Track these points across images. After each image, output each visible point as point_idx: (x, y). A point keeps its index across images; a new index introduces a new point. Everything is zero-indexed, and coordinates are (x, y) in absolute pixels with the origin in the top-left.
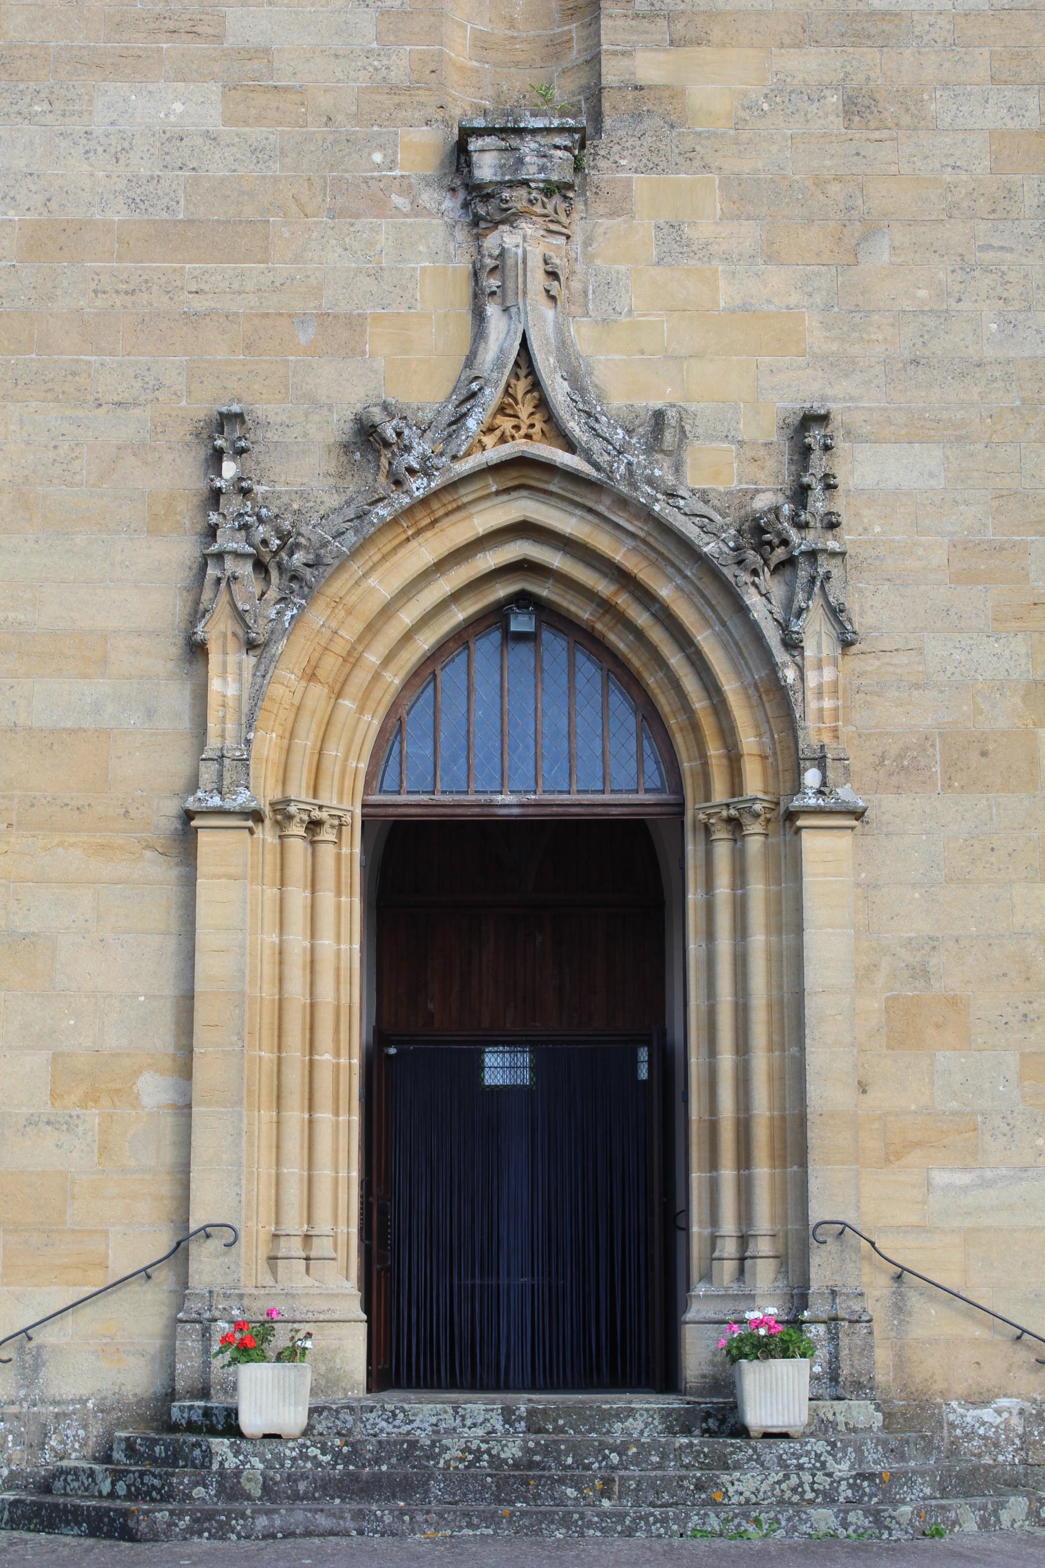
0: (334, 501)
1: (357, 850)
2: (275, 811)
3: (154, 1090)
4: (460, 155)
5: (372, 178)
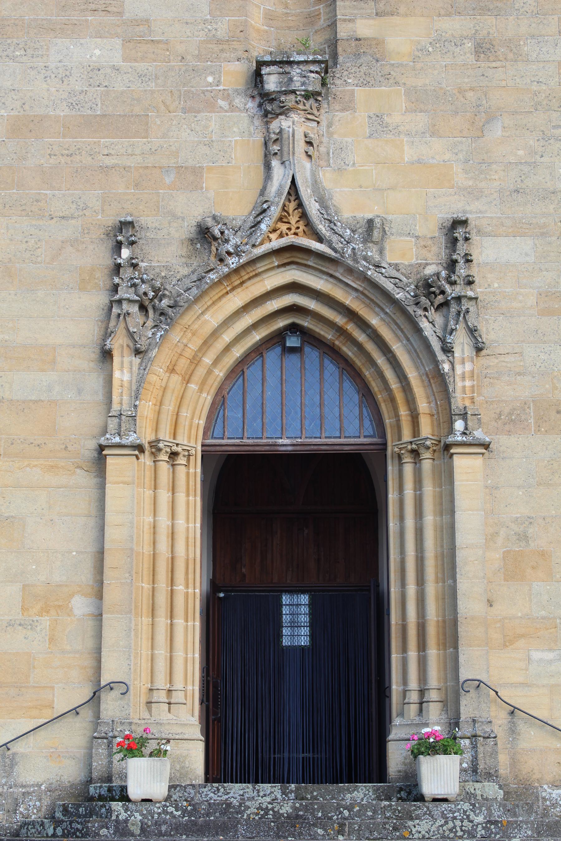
0: (185, 271)
1: (199, 470)
2: (151, 447)
3: (81, 605)
4: (257, 77)
5: (207, 91)
